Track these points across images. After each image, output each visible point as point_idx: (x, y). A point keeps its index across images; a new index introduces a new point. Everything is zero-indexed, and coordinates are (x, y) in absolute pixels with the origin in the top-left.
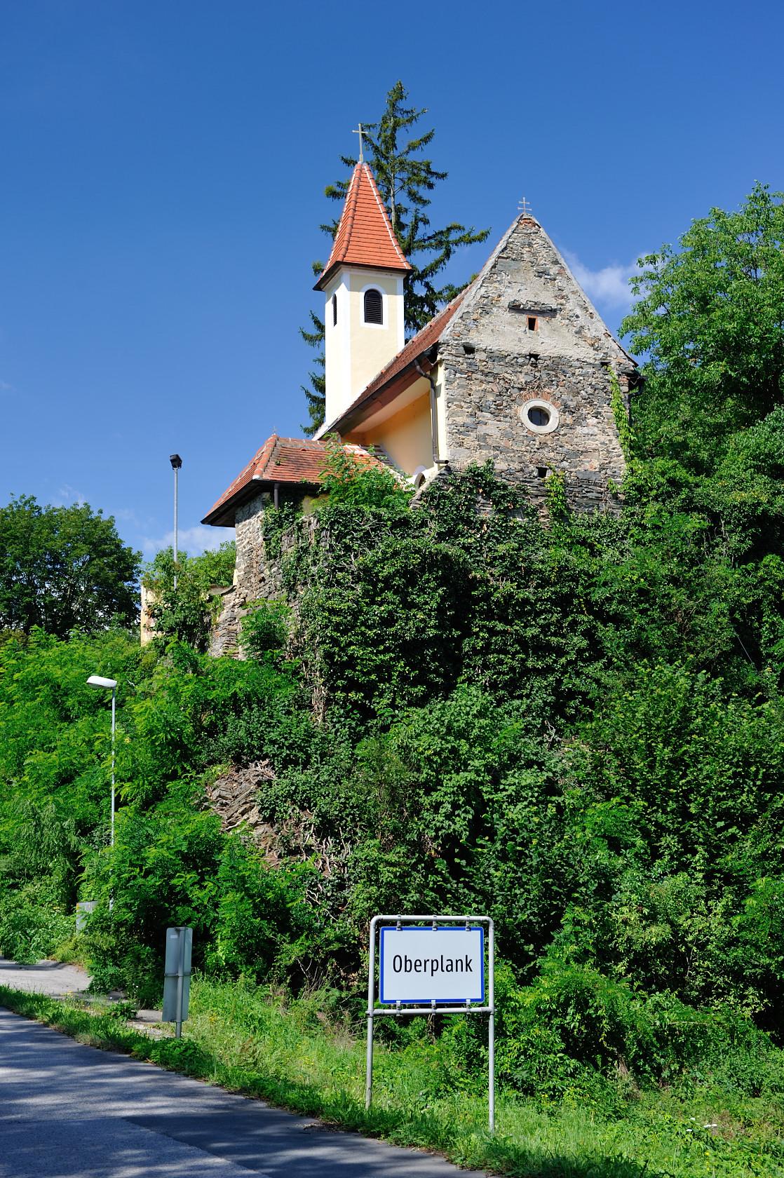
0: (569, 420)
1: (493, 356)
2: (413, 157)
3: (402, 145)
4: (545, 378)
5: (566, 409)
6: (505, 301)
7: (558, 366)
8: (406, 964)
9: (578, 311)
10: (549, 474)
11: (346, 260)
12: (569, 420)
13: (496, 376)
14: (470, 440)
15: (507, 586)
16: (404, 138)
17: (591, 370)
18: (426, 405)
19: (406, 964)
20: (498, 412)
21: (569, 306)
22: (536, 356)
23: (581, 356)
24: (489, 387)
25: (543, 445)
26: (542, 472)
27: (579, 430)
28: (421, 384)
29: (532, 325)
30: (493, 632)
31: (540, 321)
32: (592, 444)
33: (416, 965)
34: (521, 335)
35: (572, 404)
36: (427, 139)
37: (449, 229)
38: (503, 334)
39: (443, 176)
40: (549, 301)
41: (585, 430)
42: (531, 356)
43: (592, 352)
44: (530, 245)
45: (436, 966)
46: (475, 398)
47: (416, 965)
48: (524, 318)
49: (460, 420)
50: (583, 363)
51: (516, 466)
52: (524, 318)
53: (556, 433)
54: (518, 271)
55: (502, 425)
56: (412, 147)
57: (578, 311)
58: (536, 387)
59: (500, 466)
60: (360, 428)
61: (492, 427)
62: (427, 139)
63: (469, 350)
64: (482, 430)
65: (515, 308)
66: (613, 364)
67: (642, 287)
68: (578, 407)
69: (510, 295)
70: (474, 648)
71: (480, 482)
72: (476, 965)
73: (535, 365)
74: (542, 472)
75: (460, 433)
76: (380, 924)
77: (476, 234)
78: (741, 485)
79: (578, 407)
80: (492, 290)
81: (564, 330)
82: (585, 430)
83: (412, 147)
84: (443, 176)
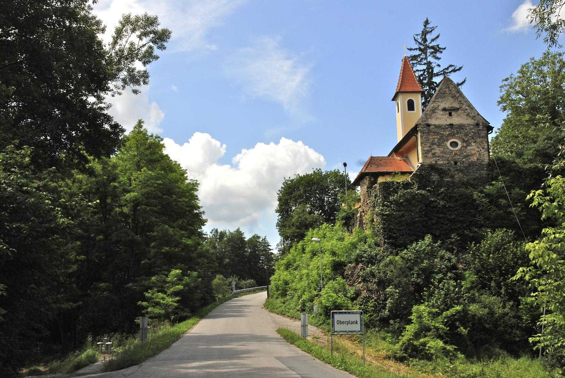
0: (465, 145)
1: (436, 126)
2: (434, 44)
3: (429, 41)
4: (455, 132)
5: (464, 141)
6: (440, 108)
7: (461, 127)
8: (340, 322)
9: (467, 108)
10: (458, 163)
11: (401, 90)
12: (465, 145)
13: (438, 133)
14: (430, 155)
15: (442, 203)
16: (429, 37)
17: (472, 127)
18: (415, 146)
19: (340, 322)
20: (439, 145)
21: (464, 107)
22: (452, 125)
23: (468, 123)
24: (435, 137)
25: (456, 154)
26: (456, 163)
27: (469, 148)
28: (414, 137)
29: (450, 114)
30: (439, 218)
31: (453, 113)
32: (473, 152)
33: (343, 323)
34: (446, 118)
35: (466, 139)
36: (437, 37)
37: (448, 67)
38: (440, 119)
39: (444, 49)
40: (456, 105)
41: (471, 148)
42: (450, 125)
43: (473, 121)
44: (449, 88)
45: (348, 323)
46: (431, 141)
47: (343, 323)
48: (447, 113)
49: (426, 149)
50: (469, 125)
51: (447, 162)
52: (447, 113)
53: (461, 149)
54: (445, 97)
55: (441, 149)
56: (433, 40)
57: (467, 108)
58: (452, 135)
59: (441, 162)
60: (401, 150)
61: (437, 150)
62: (437, 37)
63: (428, 125)
64: (433, 151)
65: (444, 110)
66: (481, 124)
67: (503, 90)
68: (468, 140)
69: (442, 105)
70: (432, 223)
71: (432, 168)
72: (359, 322)
73: (452, 128)
74: (456, 163)
75: (425, 154)
76: (333, 313)
77: (457, 68)
78: (531, 161)
79: (468, 140)
80: (435, 105)
81: (462, 115)
82: (471, 148)
83: (433, 40)
84: (444, 49)
